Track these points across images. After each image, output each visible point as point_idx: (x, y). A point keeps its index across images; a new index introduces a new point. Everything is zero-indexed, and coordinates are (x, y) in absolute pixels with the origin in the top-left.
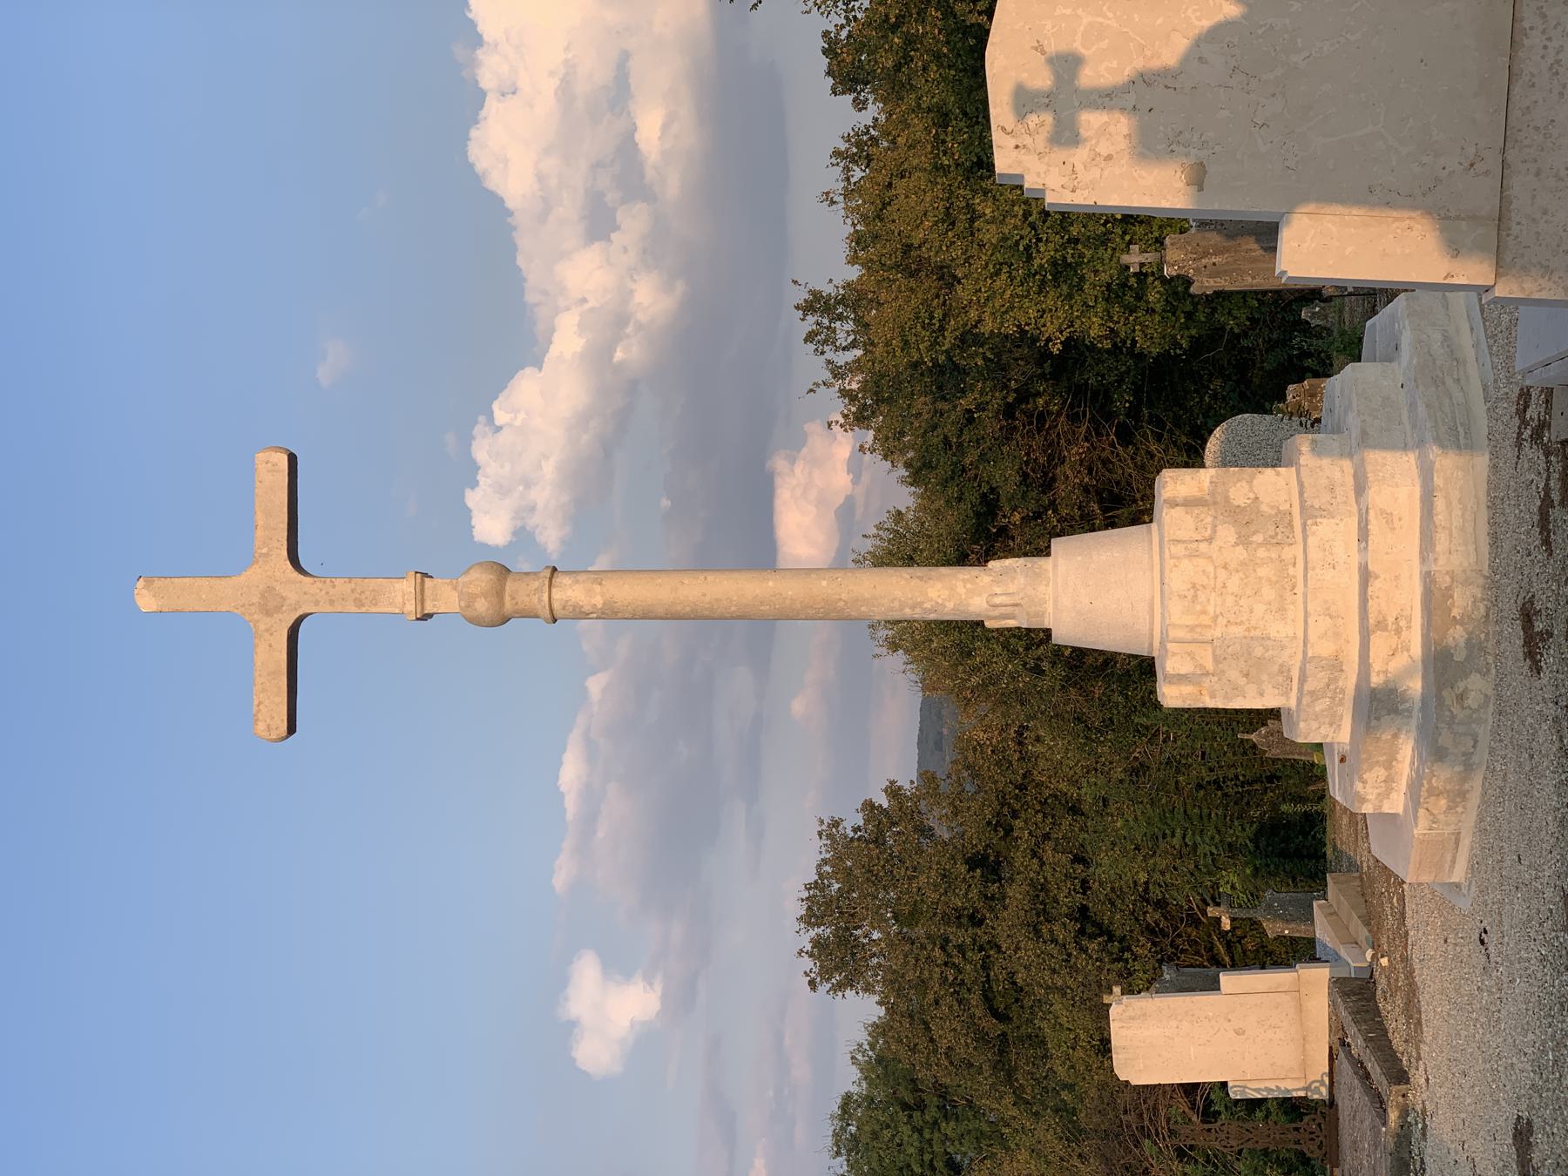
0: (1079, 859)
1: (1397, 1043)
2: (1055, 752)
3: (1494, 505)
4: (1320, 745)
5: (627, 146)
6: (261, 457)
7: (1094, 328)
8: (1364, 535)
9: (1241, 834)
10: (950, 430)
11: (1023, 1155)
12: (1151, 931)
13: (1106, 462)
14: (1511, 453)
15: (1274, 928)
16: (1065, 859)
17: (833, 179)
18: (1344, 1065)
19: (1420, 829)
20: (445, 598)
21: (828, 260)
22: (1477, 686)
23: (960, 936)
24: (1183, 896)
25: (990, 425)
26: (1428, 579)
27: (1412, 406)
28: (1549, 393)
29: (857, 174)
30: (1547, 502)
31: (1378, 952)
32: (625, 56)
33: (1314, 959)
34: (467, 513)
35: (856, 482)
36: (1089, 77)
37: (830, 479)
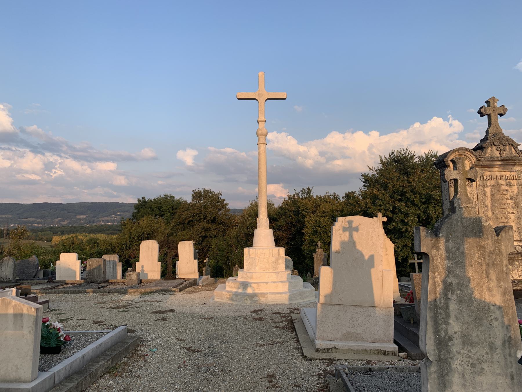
0: (215, 236)
1: (186, 290)
2: (234, 232)
3: (279, 305)
4: (237, 276)
5: (335, 158)
6: (285, 93)
7: (306, 238)
8: (274, 282)
9: (220, 264)
10: (288, 213)
11: (165, 227)
12: (203, 248)
13: (283, 240)
14: (288, 307)
15: (204, 269)
16: (215, 234)
17: (331, 193)
18: (182, 281)
19: (223, 293)
20: (261, 125)
21: (316, 193)
22: (248, 302)
23: (202, 216)
24: (209, 254)
25: (289, 220)
26: (266, 294)
27: (296, 291)
28: (299, 314)
29: (332, 197)
30: (280, 313)
31: (202, 286)
32: (350, 158)
33: (200, 276)
34: (272, 132)
35: (279, 198)
36: (355, 233)
37: (279, 193)
